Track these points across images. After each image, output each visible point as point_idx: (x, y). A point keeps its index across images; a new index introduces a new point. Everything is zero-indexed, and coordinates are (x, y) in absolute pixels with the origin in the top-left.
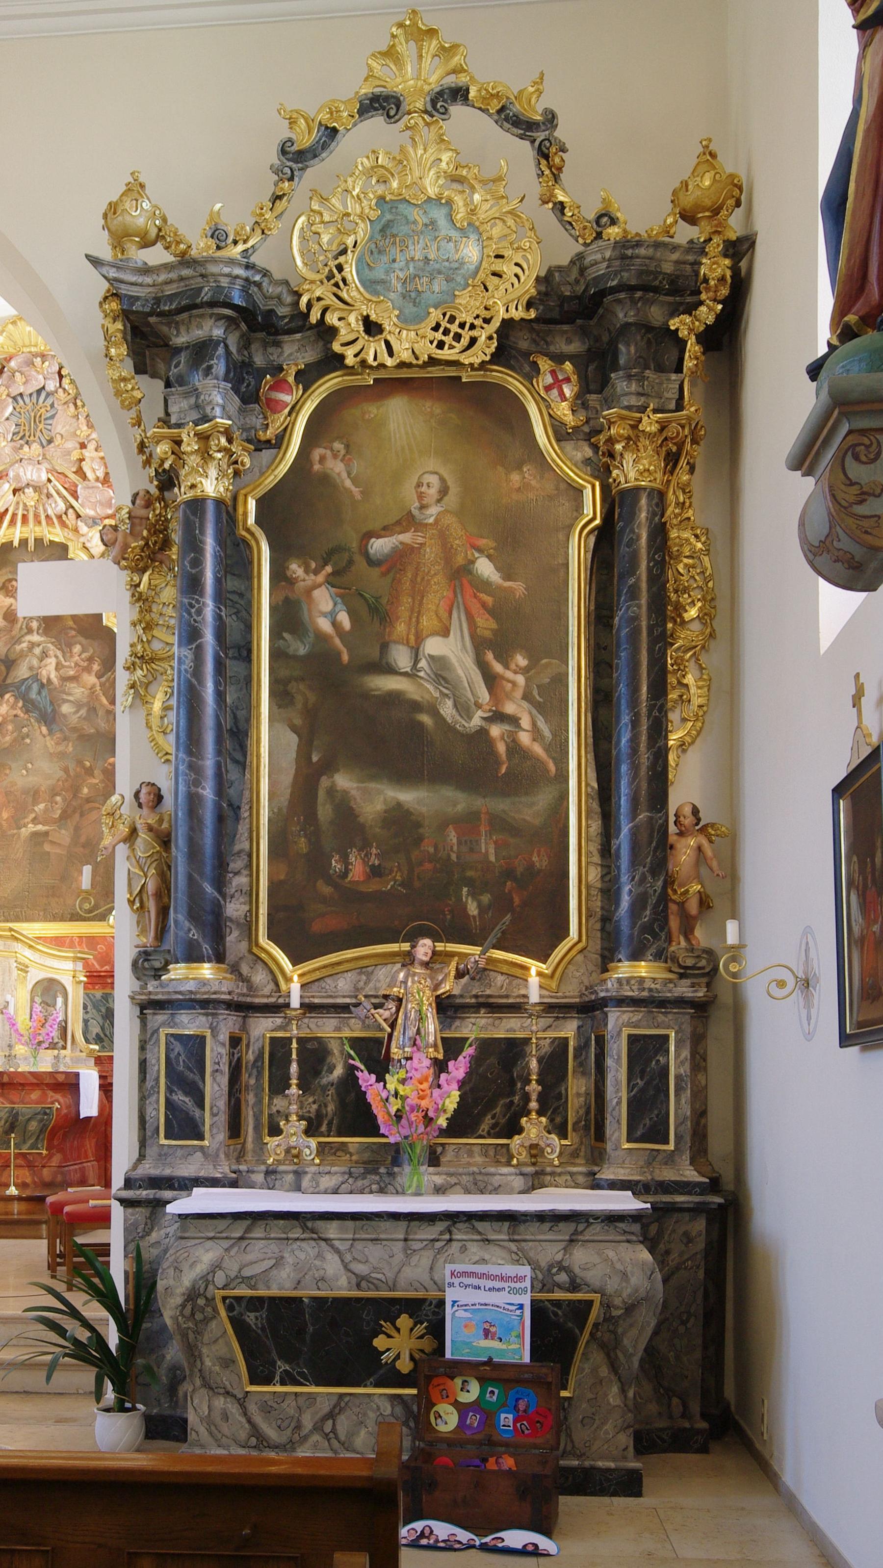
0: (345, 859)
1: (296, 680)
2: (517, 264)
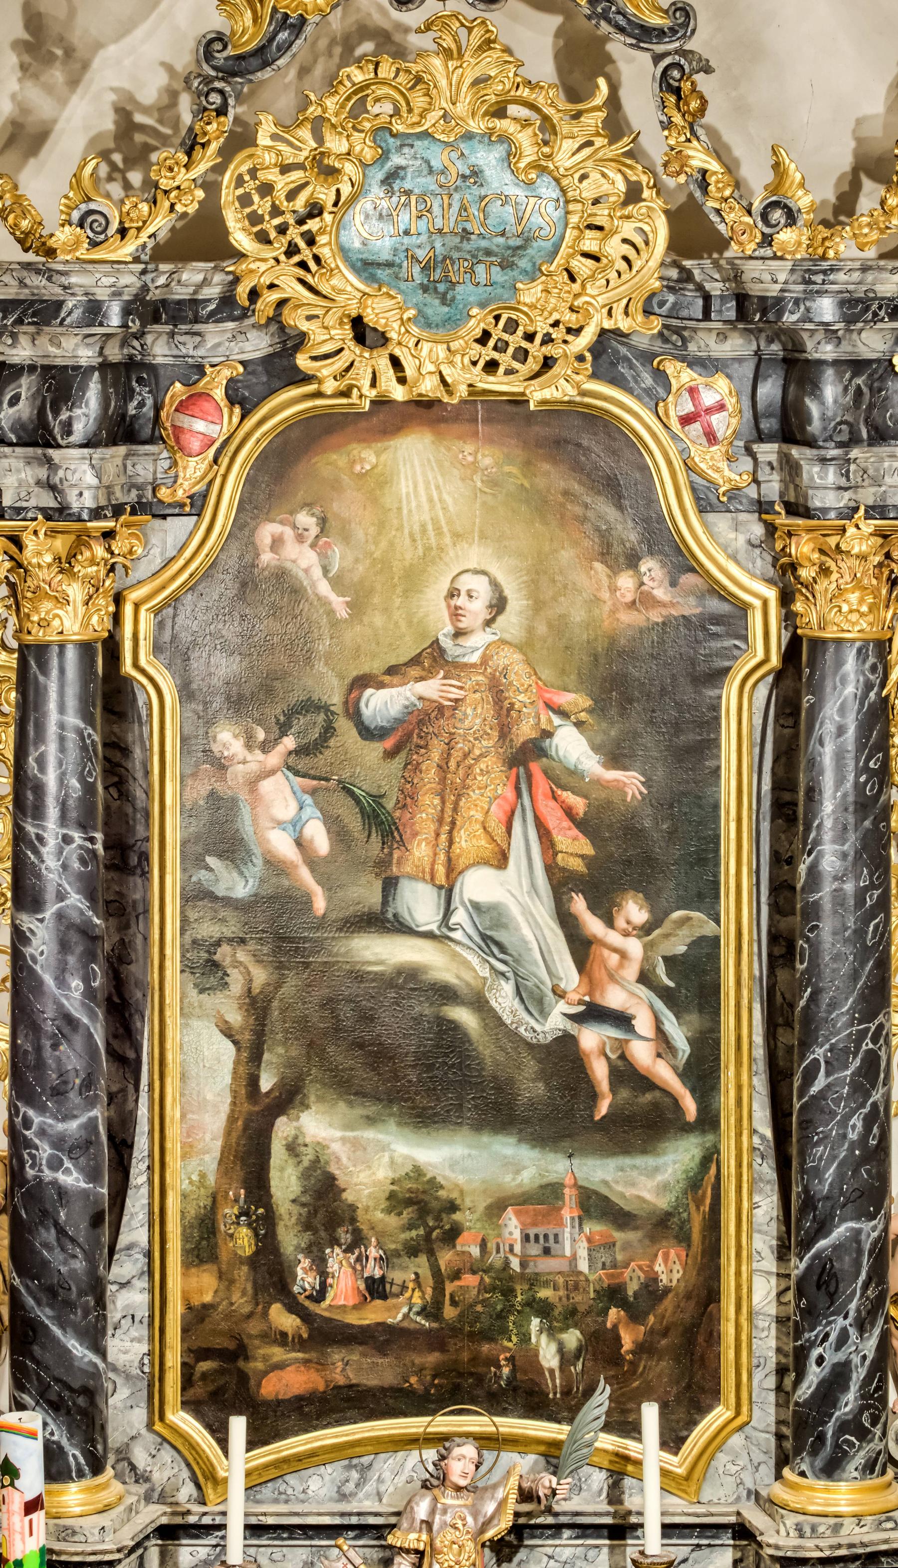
0: (320, 1266)
1: (230, 940)
2: (625, 241)
